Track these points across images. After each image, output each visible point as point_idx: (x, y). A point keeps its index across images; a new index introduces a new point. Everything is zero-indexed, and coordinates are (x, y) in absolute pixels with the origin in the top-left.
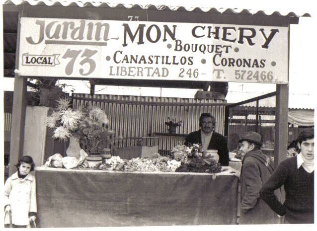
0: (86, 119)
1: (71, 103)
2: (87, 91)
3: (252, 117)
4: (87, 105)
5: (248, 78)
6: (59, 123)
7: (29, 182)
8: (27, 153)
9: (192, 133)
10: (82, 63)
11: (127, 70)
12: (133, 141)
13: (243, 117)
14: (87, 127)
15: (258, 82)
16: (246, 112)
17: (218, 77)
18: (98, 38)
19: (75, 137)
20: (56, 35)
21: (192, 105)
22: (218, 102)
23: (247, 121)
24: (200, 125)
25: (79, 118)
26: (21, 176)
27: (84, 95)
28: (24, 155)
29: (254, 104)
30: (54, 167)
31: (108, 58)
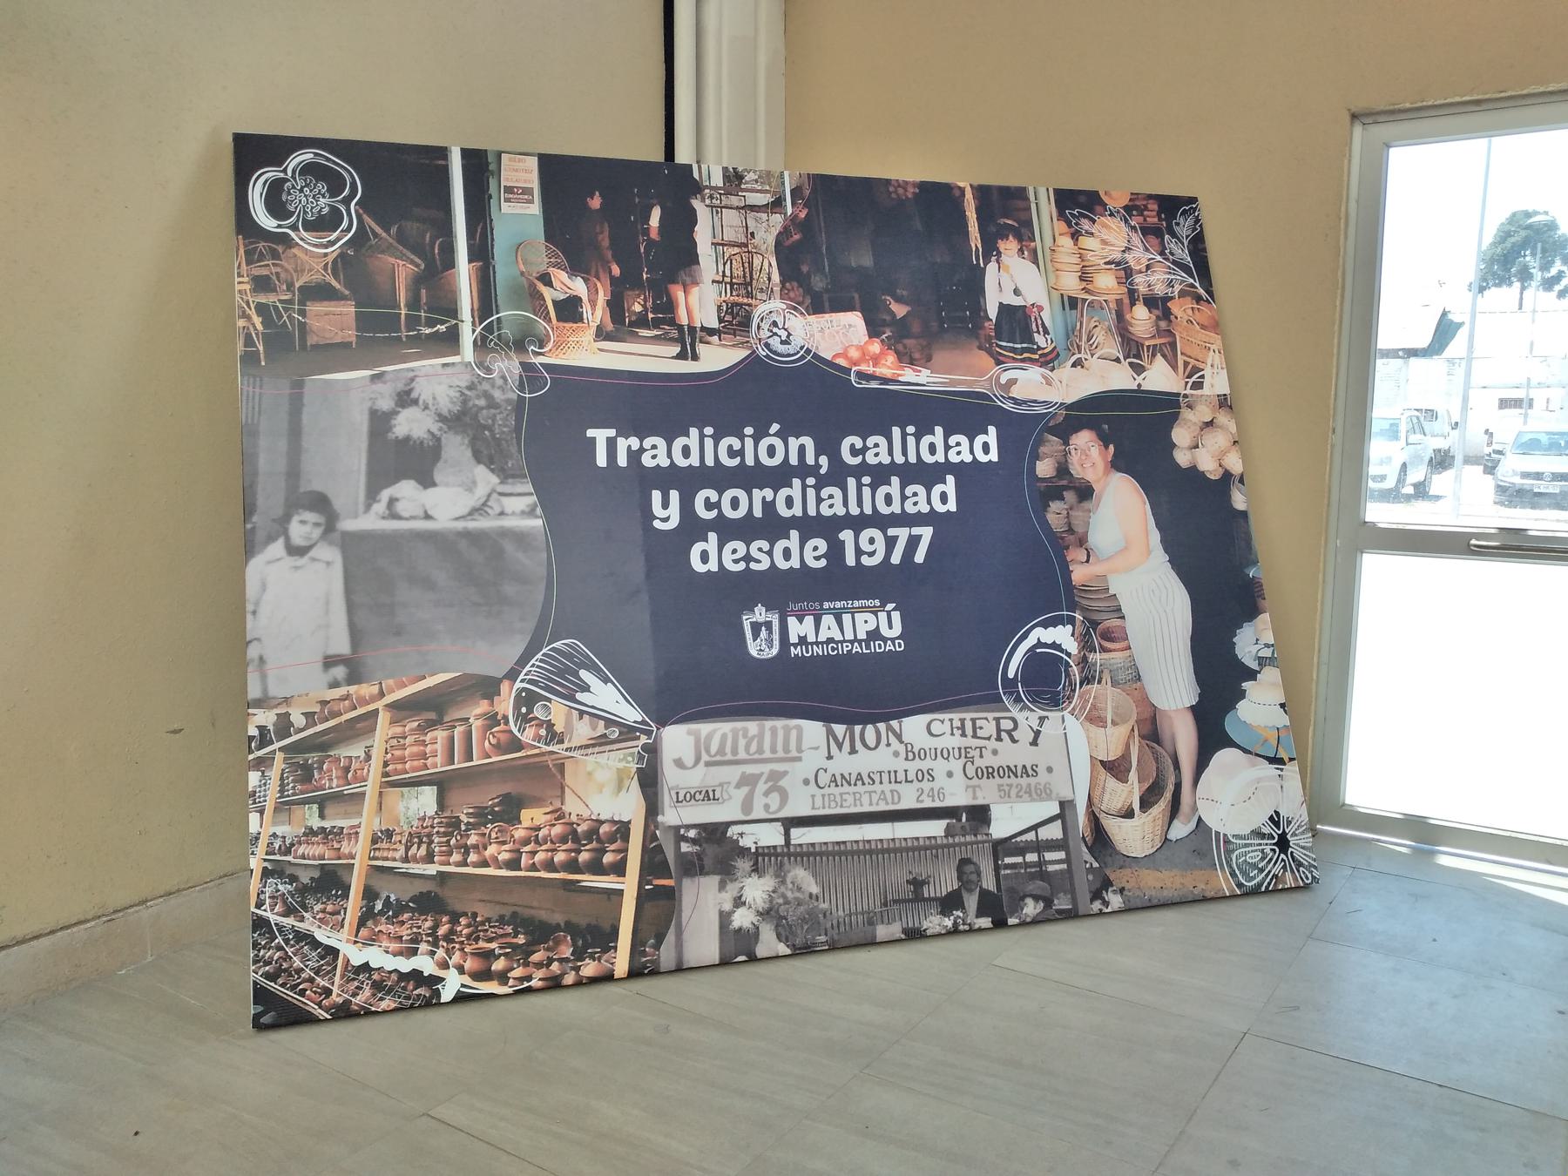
0: (782, 889)
1: (756, 863)
2: (779, 840)
3: (1032, 857)
4: (782, 865)
5: (1018, 796)
6: (739, 902)
7: (320, 566)
8: (314, 481)
9: (949, 894)
10: (766, 794)
11: (838, 799)
12: (860, 918)
13: (1019, 859)
14: (489, 407)
15: (1033, 800)
16: (1021, 850)
17: (975, 798)
18: (787, 750)
19: (456, 433)
20: (721, 751)
21: (943, 846)
22: (979, 838)
23: (1027, 865)
24: (959, 878)
25: (464, 384)
26: (295, 551)
27: (775, 847)
28: (302, 490)
29: (1031, 836)
30: (399, 518)
31: (806, 782)
